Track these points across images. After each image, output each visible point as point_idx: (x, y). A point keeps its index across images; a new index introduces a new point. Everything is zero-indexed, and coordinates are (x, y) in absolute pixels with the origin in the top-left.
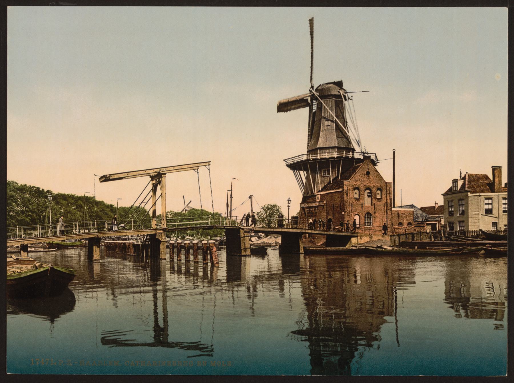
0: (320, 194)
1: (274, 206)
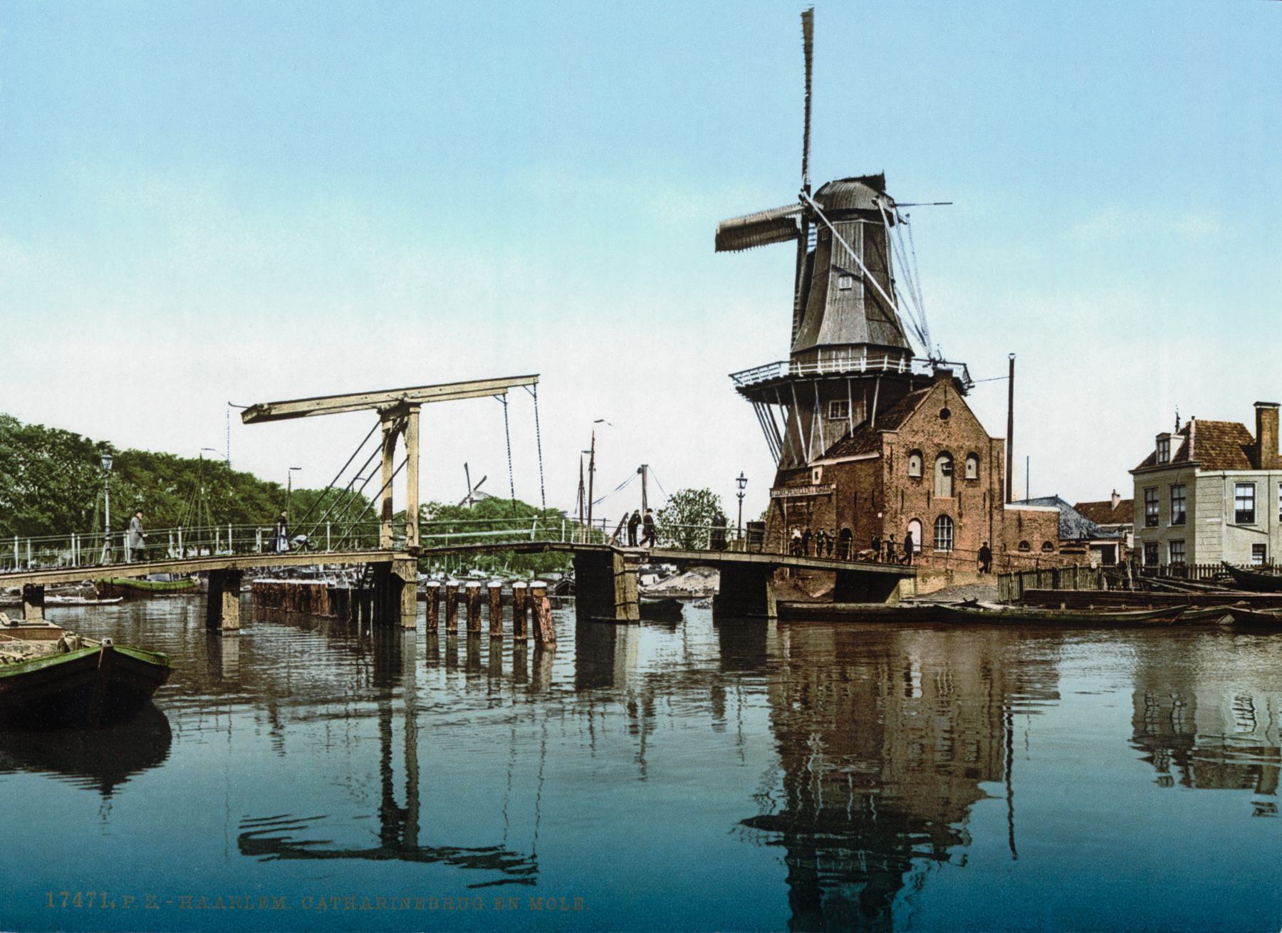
0: (823, 466)
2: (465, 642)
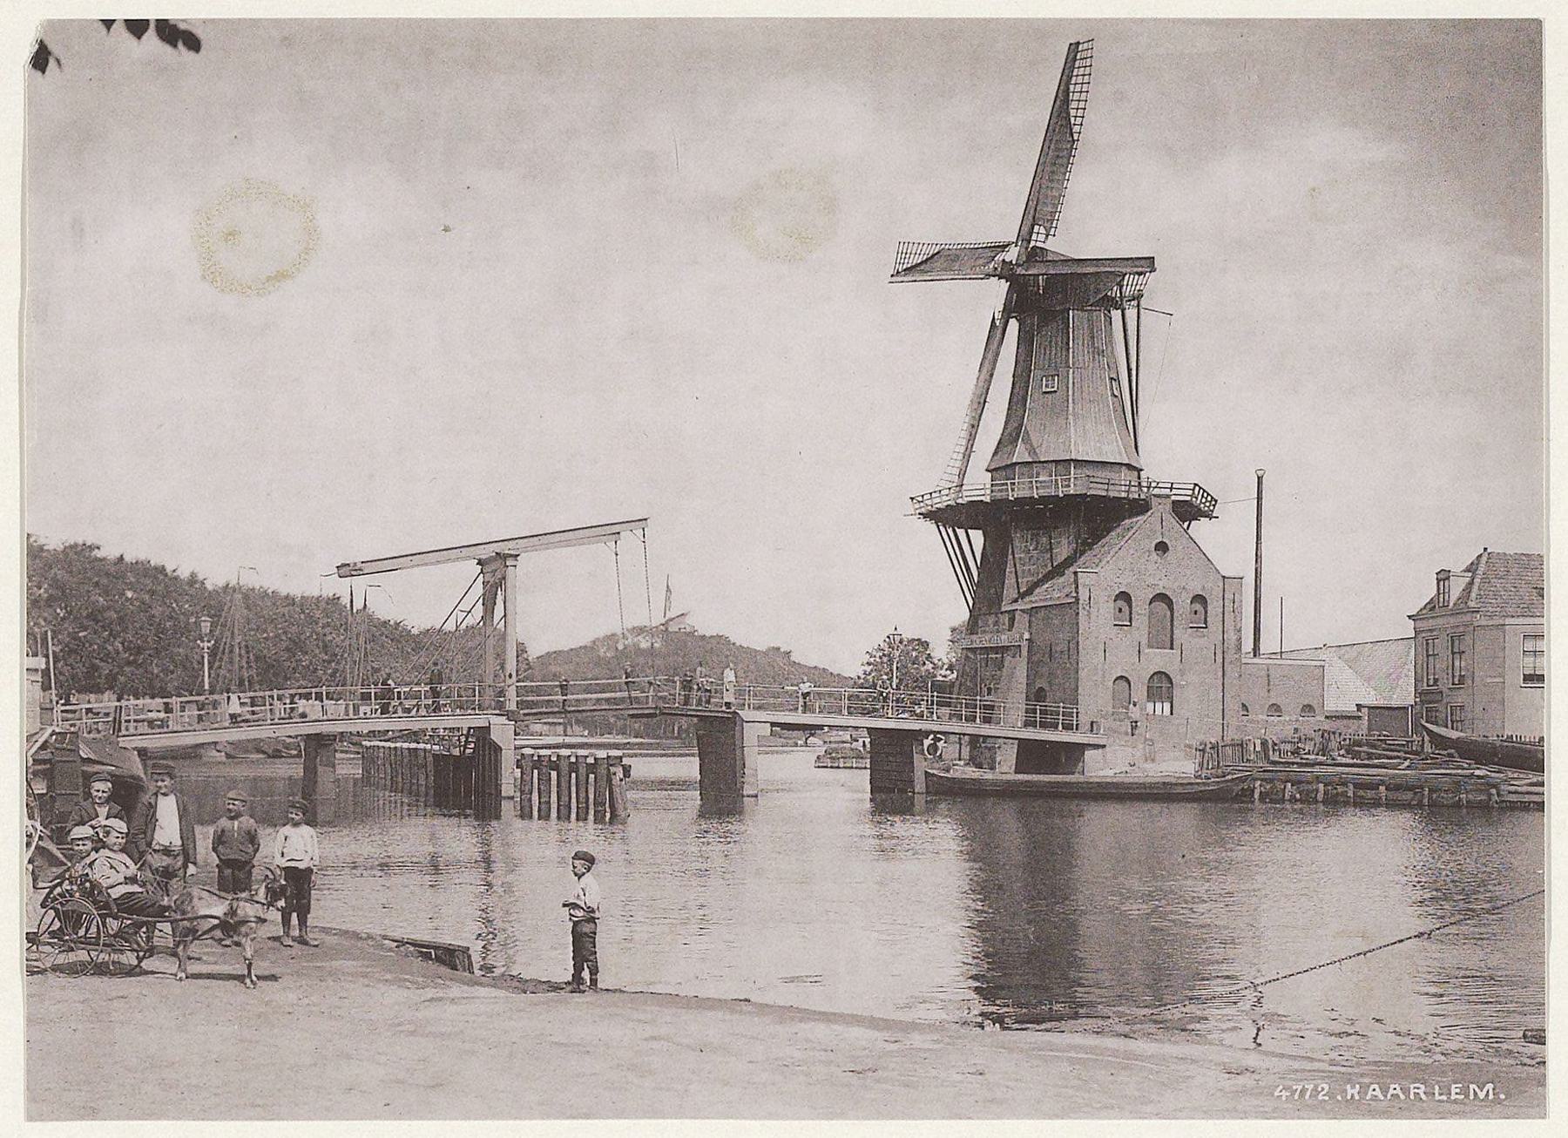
2: (302, 766)
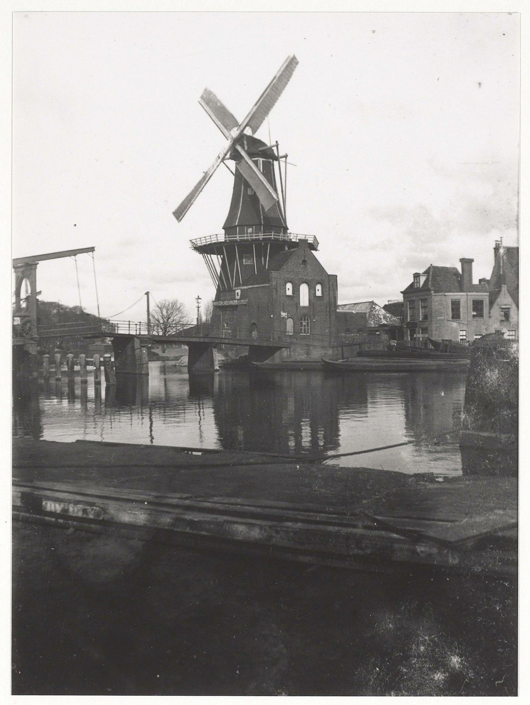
0: (241, 289)
1: (174, 304)
